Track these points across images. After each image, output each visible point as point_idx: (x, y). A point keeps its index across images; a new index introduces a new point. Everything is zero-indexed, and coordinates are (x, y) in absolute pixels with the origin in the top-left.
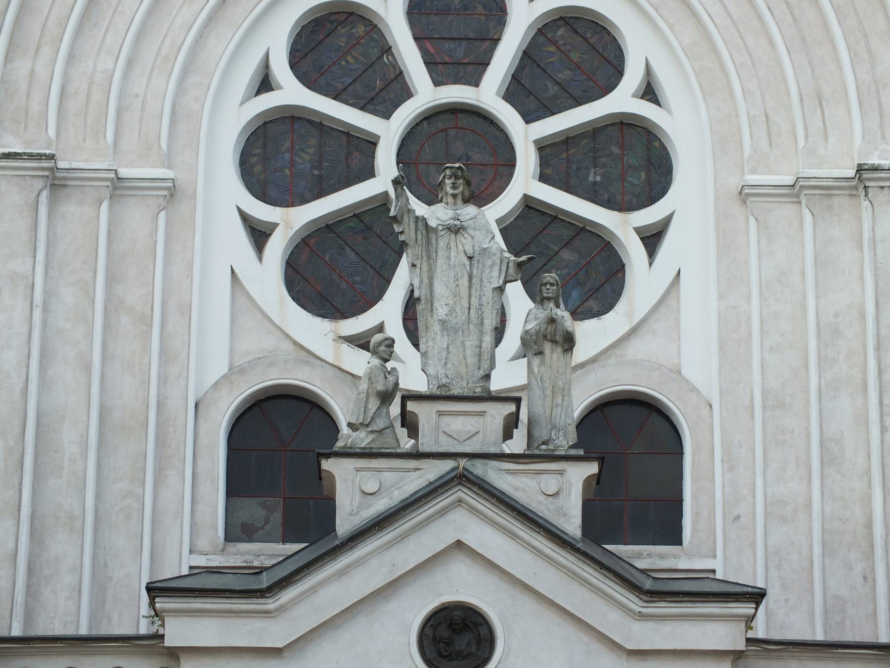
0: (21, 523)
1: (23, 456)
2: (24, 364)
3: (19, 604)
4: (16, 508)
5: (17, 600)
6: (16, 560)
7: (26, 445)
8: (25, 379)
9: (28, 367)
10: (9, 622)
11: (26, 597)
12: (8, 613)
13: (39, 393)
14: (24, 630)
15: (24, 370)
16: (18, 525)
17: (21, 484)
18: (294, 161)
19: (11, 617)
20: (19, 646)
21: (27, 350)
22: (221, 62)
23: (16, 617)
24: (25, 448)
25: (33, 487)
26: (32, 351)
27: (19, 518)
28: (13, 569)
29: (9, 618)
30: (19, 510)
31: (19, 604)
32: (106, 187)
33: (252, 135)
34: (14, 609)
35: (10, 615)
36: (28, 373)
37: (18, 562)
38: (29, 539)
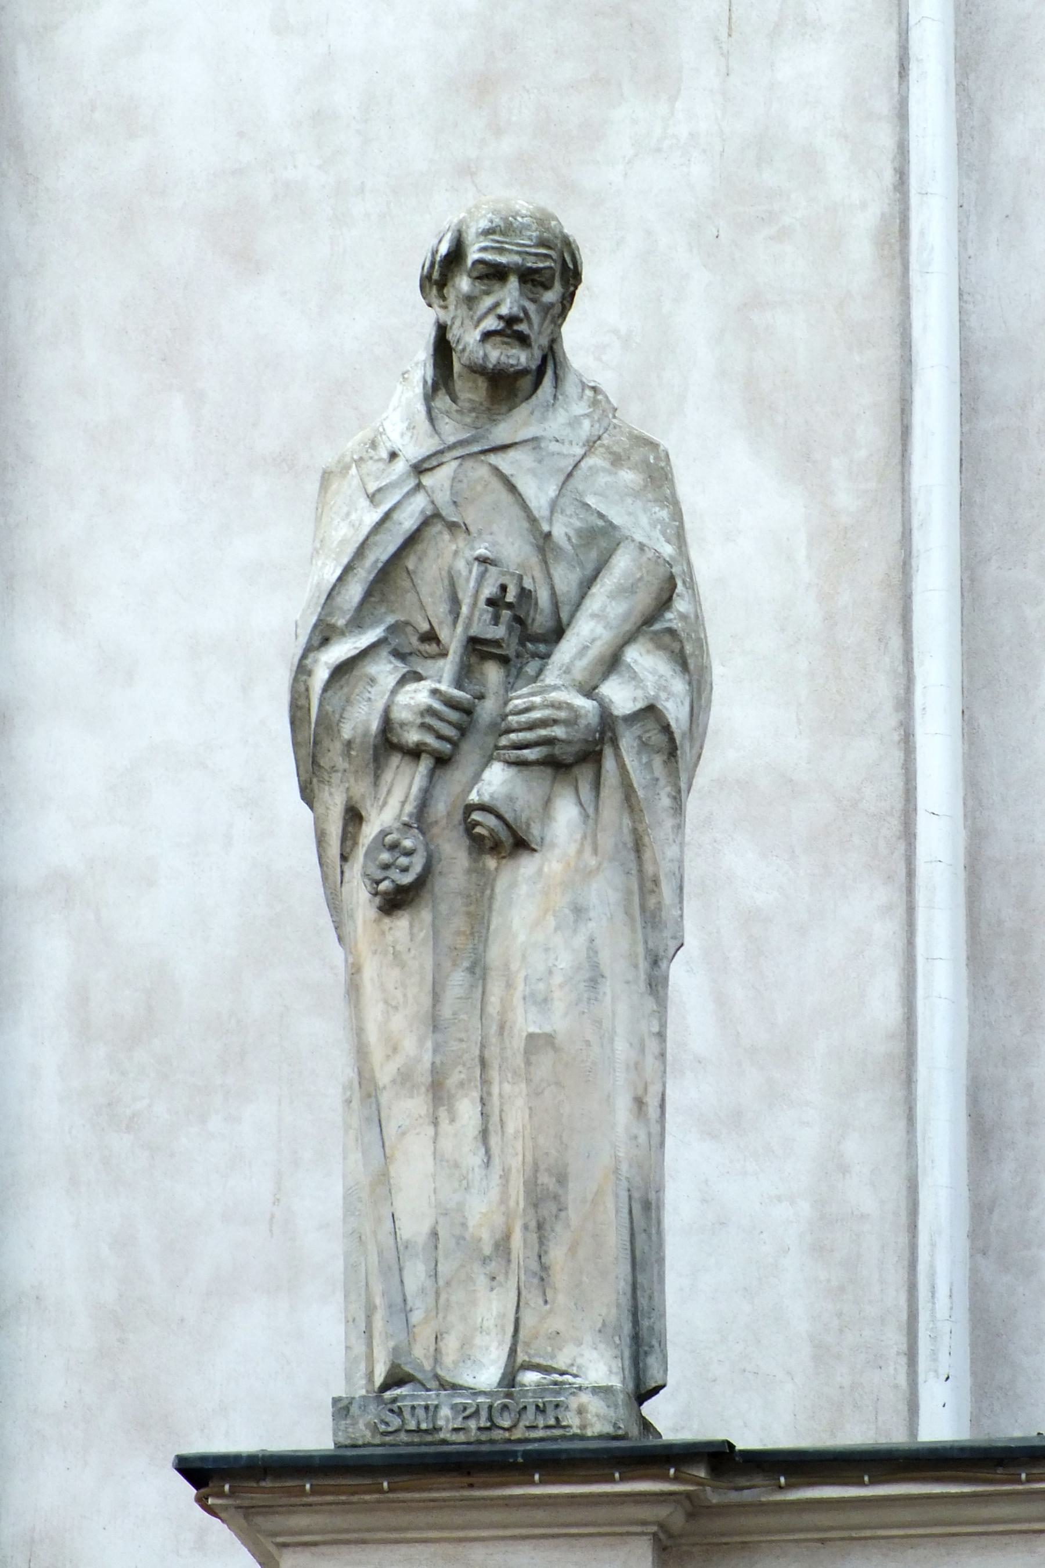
0: (921, 898)
1: (906, 567)
2: (883, 105)
3: (942, 1292)
4: (895, 823)
5: (932, 1275)
6: (909, 1081)
7: (918, 509)
8: (889, 177)
9: (902, 115)
10: (902, 1380)
11: (972, 1256)
12: (894, 1340)
13: (963, 243)
14: (975, 1420)
15: (885, 138)
16: (911, 909)
17: (905, 704)
18: (522, 1365)
19: (912, 1356)
20: (967, 1489)
21: (893, 36)
22: (915, 92)
23: (934, 1355)
24: (915, 523)
25: (967, 715)
26: (914, 35)
27: (911, 874)
28: (902, 1124)
29: (903, 1360)
30: (908, 833)
31: (942, 1292)
32: (716, 234)
33: (963, 426)
34: (923, 1318)
35: (904, 1347)
36: (903, 149)
37: (921, 1088)
38: (964, 972)
